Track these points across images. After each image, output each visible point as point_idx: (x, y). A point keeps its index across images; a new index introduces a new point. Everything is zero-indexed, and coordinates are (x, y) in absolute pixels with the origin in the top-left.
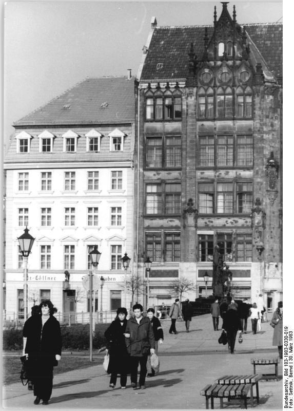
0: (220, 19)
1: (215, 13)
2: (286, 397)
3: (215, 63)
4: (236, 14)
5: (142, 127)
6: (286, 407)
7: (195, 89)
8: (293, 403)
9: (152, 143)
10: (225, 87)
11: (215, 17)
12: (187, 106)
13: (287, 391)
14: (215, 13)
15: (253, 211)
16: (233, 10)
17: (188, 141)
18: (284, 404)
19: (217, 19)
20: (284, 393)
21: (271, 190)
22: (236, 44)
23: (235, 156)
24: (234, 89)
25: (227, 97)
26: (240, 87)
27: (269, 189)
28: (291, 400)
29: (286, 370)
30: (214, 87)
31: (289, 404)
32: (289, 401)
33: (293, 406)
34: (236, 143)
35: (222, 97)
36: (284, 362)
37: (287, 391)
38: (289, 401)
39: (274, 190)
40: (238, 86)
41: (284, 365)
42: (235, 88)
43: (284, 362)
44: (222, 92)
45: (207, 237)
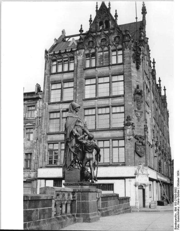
0: (100, 8)
1: (97, 6)
2: (176, 223)
3: (96, 34)
4: (110, 4)
5: (49, 77)
6: (175, 229)
7: (83, 50)
8: (179, 227)
9: (54, 87)
10: (103, 47)
11: (97, 8)
12: (78, 61)
13: (176, 220)
14: (97, 6)
15: (126, 125)
16: (115, 13)
17: (78, 83)
18: (174, 227)
19: (98, 9)
20: (174, 221)
21: (138, 110)
22: (111, 21)
23: (111, 89)
24: (109, 47)
25: (105, 53)
26: (113, 46)
27: (136, 109)
28: (178, 225)
29: (176, 208)
30: (95, 47)
31: (177, 227)
32: (177, 225)
33: (179, 228)
34: (111, 80)
35: (101, 53)
36: (174, 203)
37: (176, 220)
38: (177, 225)
39: (140, 111)
40: (112, 45)
41: (174, 205)
42: (110, 46)
43: (174, 203)
44: (102, 50)
45: (25, 138)
